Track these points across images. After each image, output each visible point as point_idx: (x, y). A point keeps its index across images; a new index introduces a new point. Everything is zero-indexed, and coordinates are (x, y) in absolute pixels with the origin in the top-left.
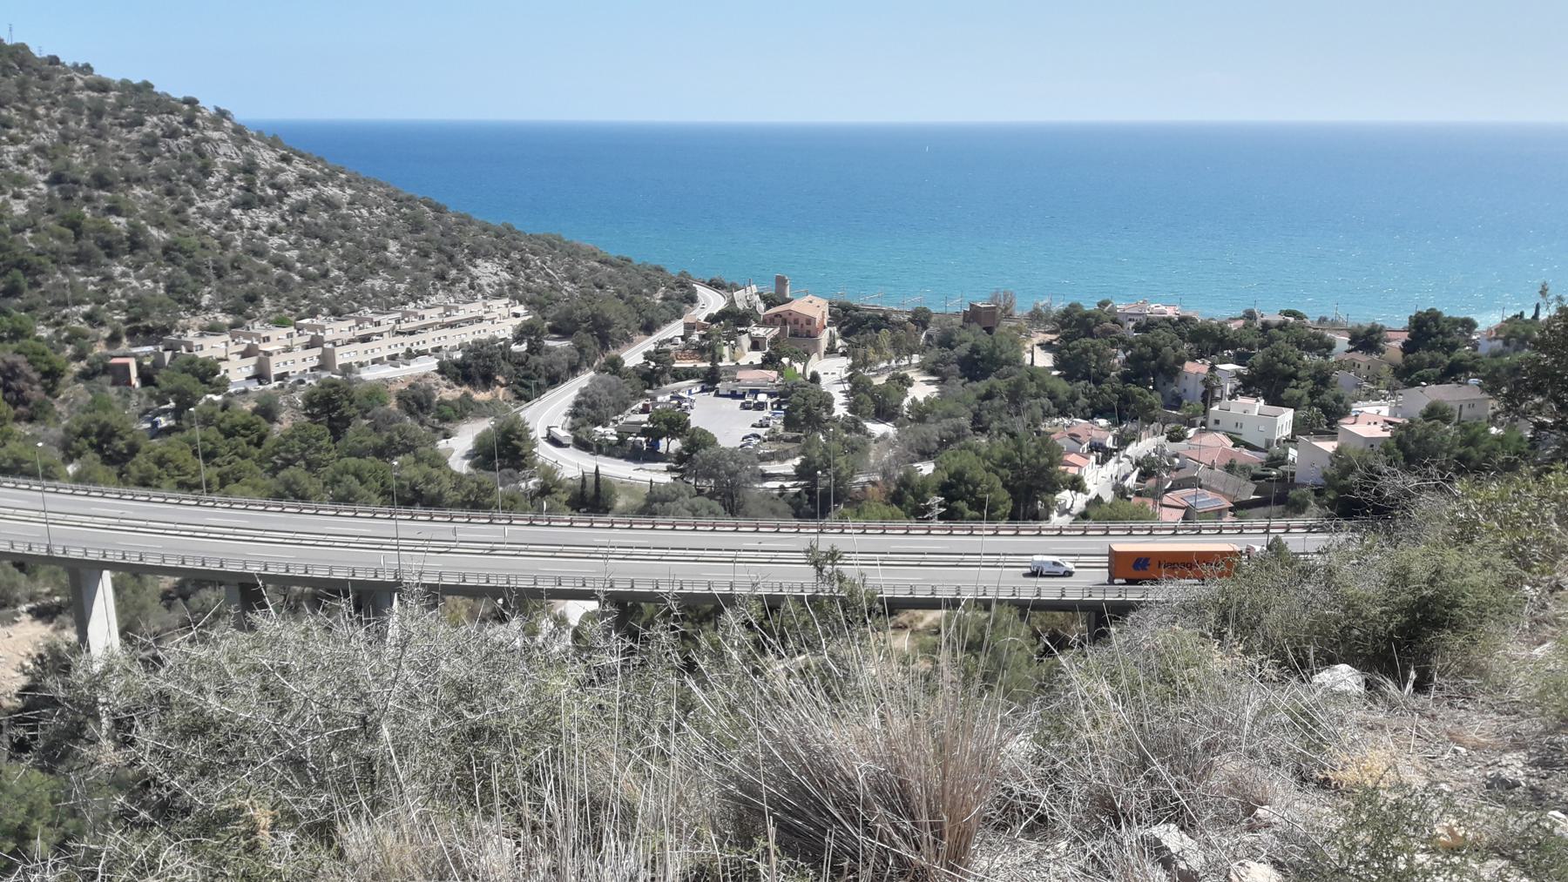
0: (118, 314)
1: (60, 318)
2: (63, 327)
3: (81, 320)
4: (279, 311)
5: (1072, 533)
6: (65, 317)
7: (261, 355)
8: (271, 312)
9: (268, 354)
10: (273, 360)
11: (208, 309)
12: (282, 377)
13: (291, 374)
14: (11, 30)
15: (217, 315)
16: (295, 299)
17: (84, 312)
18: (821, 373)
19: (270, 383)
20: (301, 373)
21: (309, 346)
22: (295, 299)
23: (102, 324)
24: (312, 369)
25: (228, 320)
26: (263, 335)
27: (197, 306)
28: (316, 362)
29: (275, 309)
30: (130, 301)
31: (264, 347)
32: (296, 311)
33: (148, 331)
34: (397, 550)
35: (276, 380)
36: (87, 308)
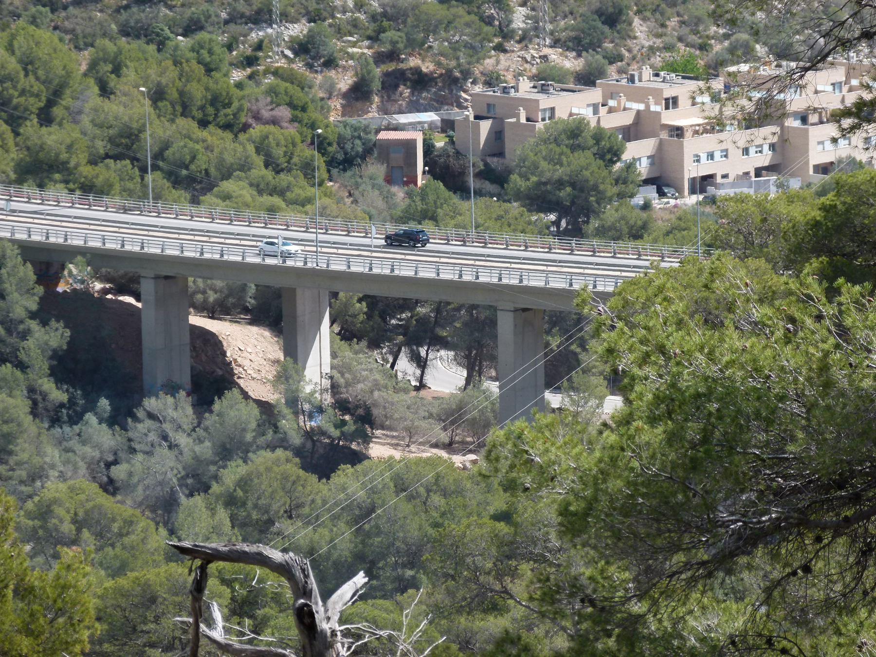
0: (354, 44)
1: (249, 52)
2: (261, 68)
3: (288, 53)
4: (669, 48)
5: (495, 246)
6: (259, 46)
7: (664, 135)
8: (652, 49)
9: (678, 132)
10: (691, 146)
11: (524, 39)
12: (703, 183)
13: (719, 180)
14: (167, 278)
15: (546, 51)
16: (699, 21)
17: (293, 39)
18: (263, 168)
19: (682, 196)
20: (738, 177)
21: (750, 122)
22: (699, 21)
23: (330, 63)
24: (758, 172)
25: (571, 63)
26: (667, 94)
27: (505, 33)
28: (765, 158)
29: (658, 42)
30: (373, 18)
31: (671, 118)
32: (703, 47)
33: (420, 81)
34: (316, 252)
35: (693, 191)
36: (298, 30)
